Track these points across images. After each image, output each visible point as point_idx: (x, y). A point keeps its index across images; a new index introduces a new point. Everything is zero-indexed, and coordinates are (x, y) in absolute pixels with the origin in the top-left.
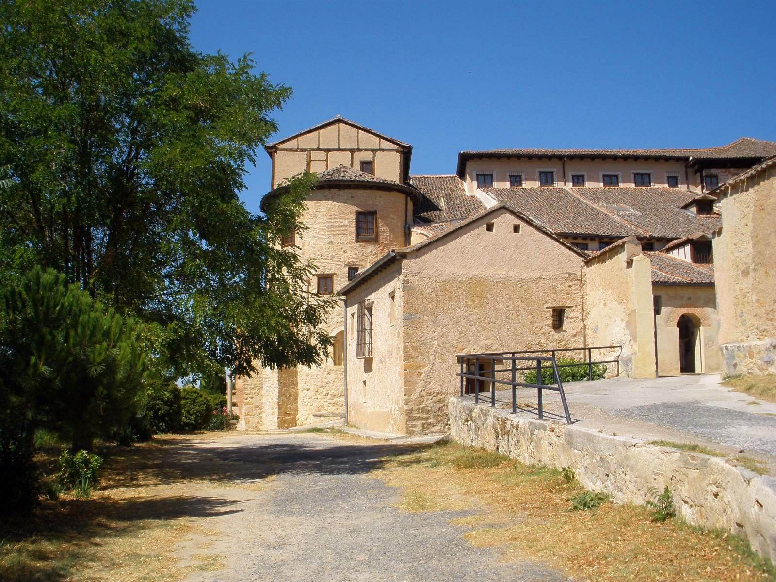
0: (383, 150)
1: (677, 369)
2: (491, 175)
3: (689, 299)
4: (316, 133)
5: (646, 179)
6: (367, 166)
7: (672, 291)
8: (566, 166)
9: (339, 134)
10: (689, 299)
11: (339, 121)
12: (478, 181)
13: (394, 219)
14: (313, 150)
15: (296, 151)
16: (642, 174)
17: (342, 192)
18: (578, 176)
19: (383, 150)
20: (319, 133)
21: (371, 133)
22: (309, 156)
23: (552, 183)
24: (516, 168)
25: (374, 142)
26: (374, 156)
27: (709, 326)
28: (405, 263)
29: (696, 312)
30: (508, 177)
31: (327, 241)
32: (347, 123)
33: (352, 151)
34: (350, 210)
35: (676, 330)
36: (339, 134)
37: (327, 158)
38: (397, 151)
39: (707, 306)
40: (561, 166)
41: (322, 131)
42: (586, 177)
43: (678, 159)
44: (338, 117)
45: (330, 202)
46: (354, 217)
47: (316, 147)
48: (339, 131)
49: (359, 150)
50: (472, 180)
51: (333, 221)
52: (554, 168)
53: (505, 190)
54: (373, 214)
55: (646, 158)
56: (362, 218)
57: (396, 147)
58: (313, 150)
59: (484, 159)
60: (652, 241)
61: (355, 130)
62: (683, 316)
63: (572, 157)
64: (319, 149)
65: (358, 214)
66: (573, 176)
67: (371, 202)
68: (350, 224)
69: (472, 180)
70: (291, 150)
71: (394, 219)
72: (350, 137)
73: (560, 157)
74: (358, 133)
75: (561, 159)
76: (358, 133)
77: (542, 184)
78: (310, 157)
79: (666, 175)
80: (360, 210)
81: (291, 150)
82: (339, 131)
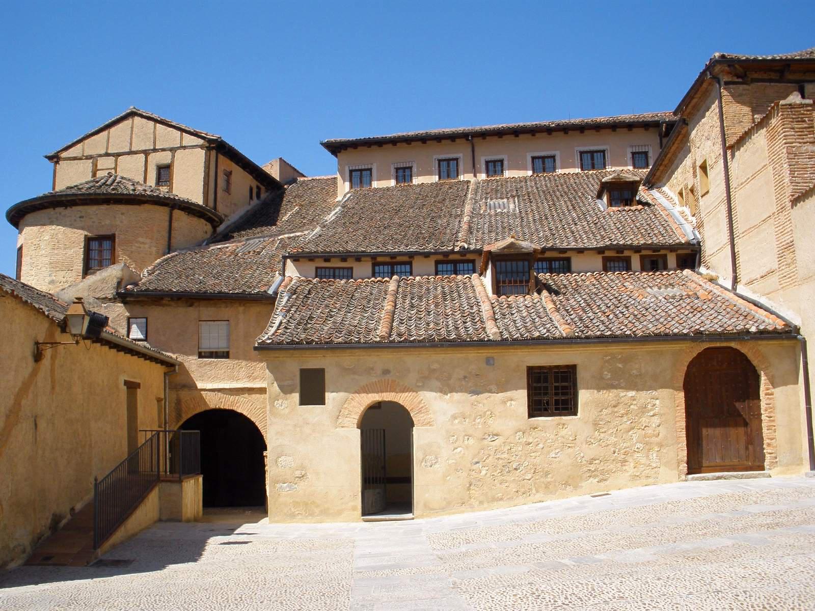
0: (185, 148)
1: (354, 509)
2: (370, 170)
3: (386, 372)
4: (105, 133)
5: (548, 162)
6: (164, 172)
7: (347, 359)
8: (476, 149)
9: (132, 131)
10: (386, 372)
11: (132, 114)
12: (351, 181)
13: (143, 243)
14: (100, 156)
15: (81, 159)
16: (592, 153)
17: (69, 211)
18: (494, 162)
19: (185, 148)
20: (109, 133)
21: (722, 121)
22: (95, 165)
23: (554, 169)
24: (401, 156)
25: (170, 137)
26: (173, 157)
27: (429, 424)
28: (87, 309)
29: (403, 399)
30: (393, 171)
31: (48, 279)
32: (142, 116)
33: (146, 153)
34: (77, 237)
35: (355, 436)
36: (132, 131)
37: (116, 165)
38: (201, 147)
39: (422, 388)
40: (469, 150)
41: (113, 130)
42: (505, 163)
43: (646, 125)
44: (131, 108)
45: (54, 227)
46: (82, 245)
47: (103, 152)
48: (132, 128)
49: (155, 150)
50: (344, 181)
51: (56, 251)
52: (461, 152)
53: (388, 189)
54: (111, 238)
55: (597, 127)
56: (94, 245)
57: (201, 142)
58: (100, 156)
59: (360, 148)
60: (627, 253)
61: (151, 123)
62: (376, 407)
63: (484, 135)
64: (107, 155)
65: (88, 240)
66: (487, 163)
67: (108, 222)
68: (77, 254)
69: (344, 181)
70: (75, 159)
71: (143, 243)
72: (145, 134)
73: (465, 136)
74: (155, 128)
75: (472, 138)
76: (155, 128)
77: (397, 182)
78: (96, 166)
79: (629, 151)
80: (90, 235)
81: (75, 159)
82: (132, 128)
